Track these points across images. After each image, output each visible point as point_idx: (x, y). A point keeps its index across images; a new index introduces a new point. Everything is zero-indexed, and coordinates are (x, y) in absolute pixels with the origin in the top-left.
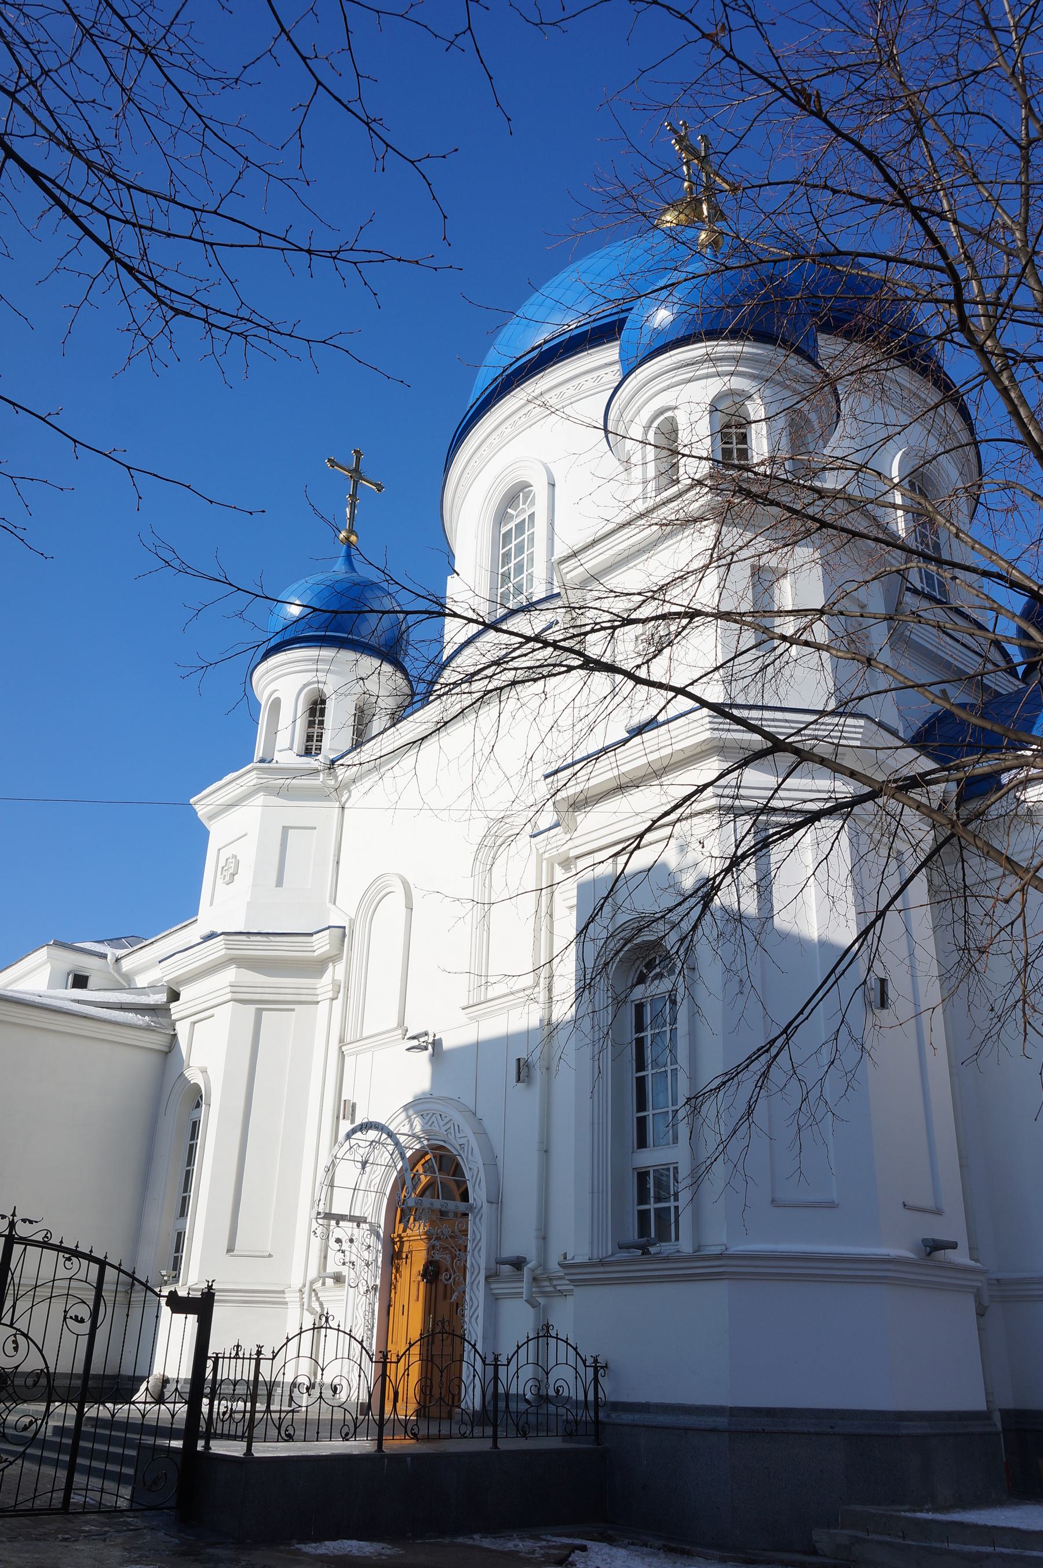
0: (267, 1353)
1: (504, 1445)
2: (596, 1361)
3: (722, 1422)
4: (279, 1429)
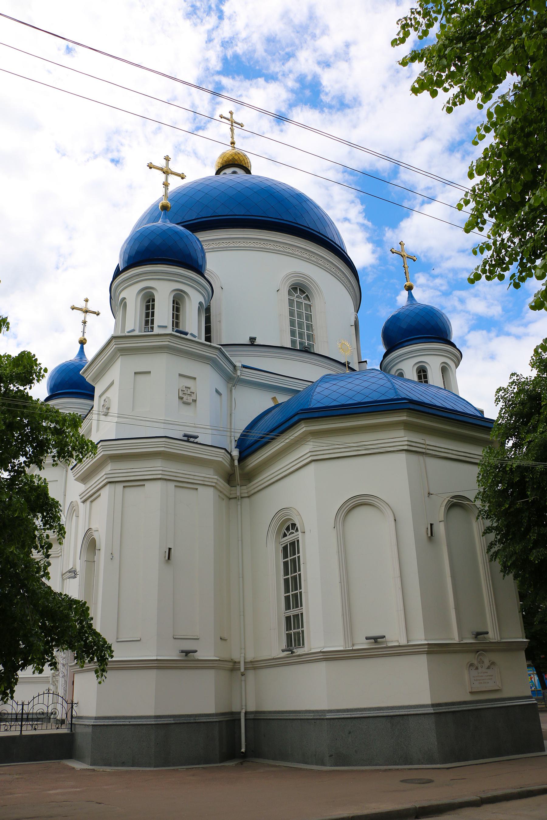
0: (26, 703)
1: (24, 733)
2: (23, 703)
3: (431, 710)
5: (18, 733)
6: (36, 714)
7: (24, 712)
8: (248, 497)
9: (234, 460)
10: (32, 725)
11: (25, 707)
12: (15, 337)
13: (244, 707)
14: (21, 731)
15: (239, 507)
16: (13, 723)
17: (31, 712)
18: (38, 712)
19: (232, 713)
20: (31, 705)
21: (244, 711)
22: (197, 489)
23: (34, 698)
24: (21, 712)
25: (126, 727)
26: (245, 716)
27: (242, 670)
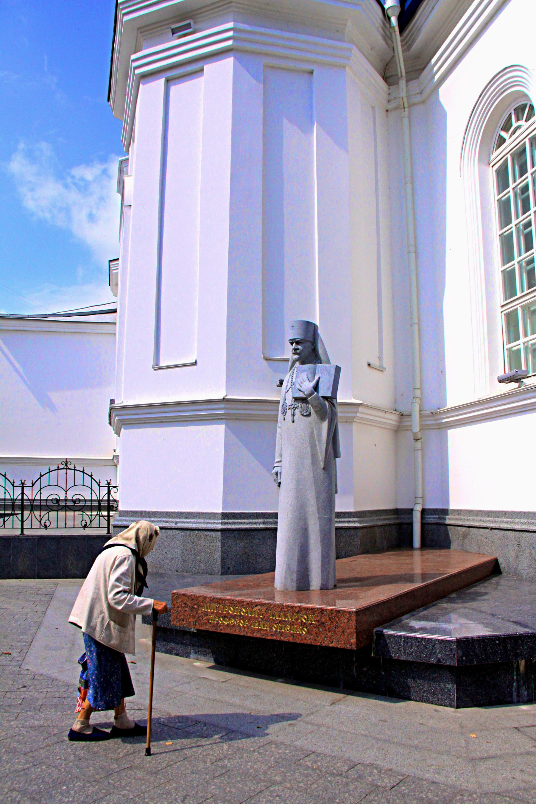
1: (27, 532)
4: (40, 522)
5: (18, 532)
6: (46, 500)
7: (25, 497)
8: (423, 102)
9: (389, 19)
10: (91, 515)
11: (27, 491)
12: (519, 577)
13: (420, 501)
14: (22, 528)
15: (406, 121)
16: (94, 513)
17: (38, 497)
18: (50, 498)
19: (397, 512)
20: (37, 486)
21: (418, 508)
22: (312, 73)
23: (41, 476)
24: (20, 497)
25: (170, 532)
26: (422, 518)
27: (416, 429)
